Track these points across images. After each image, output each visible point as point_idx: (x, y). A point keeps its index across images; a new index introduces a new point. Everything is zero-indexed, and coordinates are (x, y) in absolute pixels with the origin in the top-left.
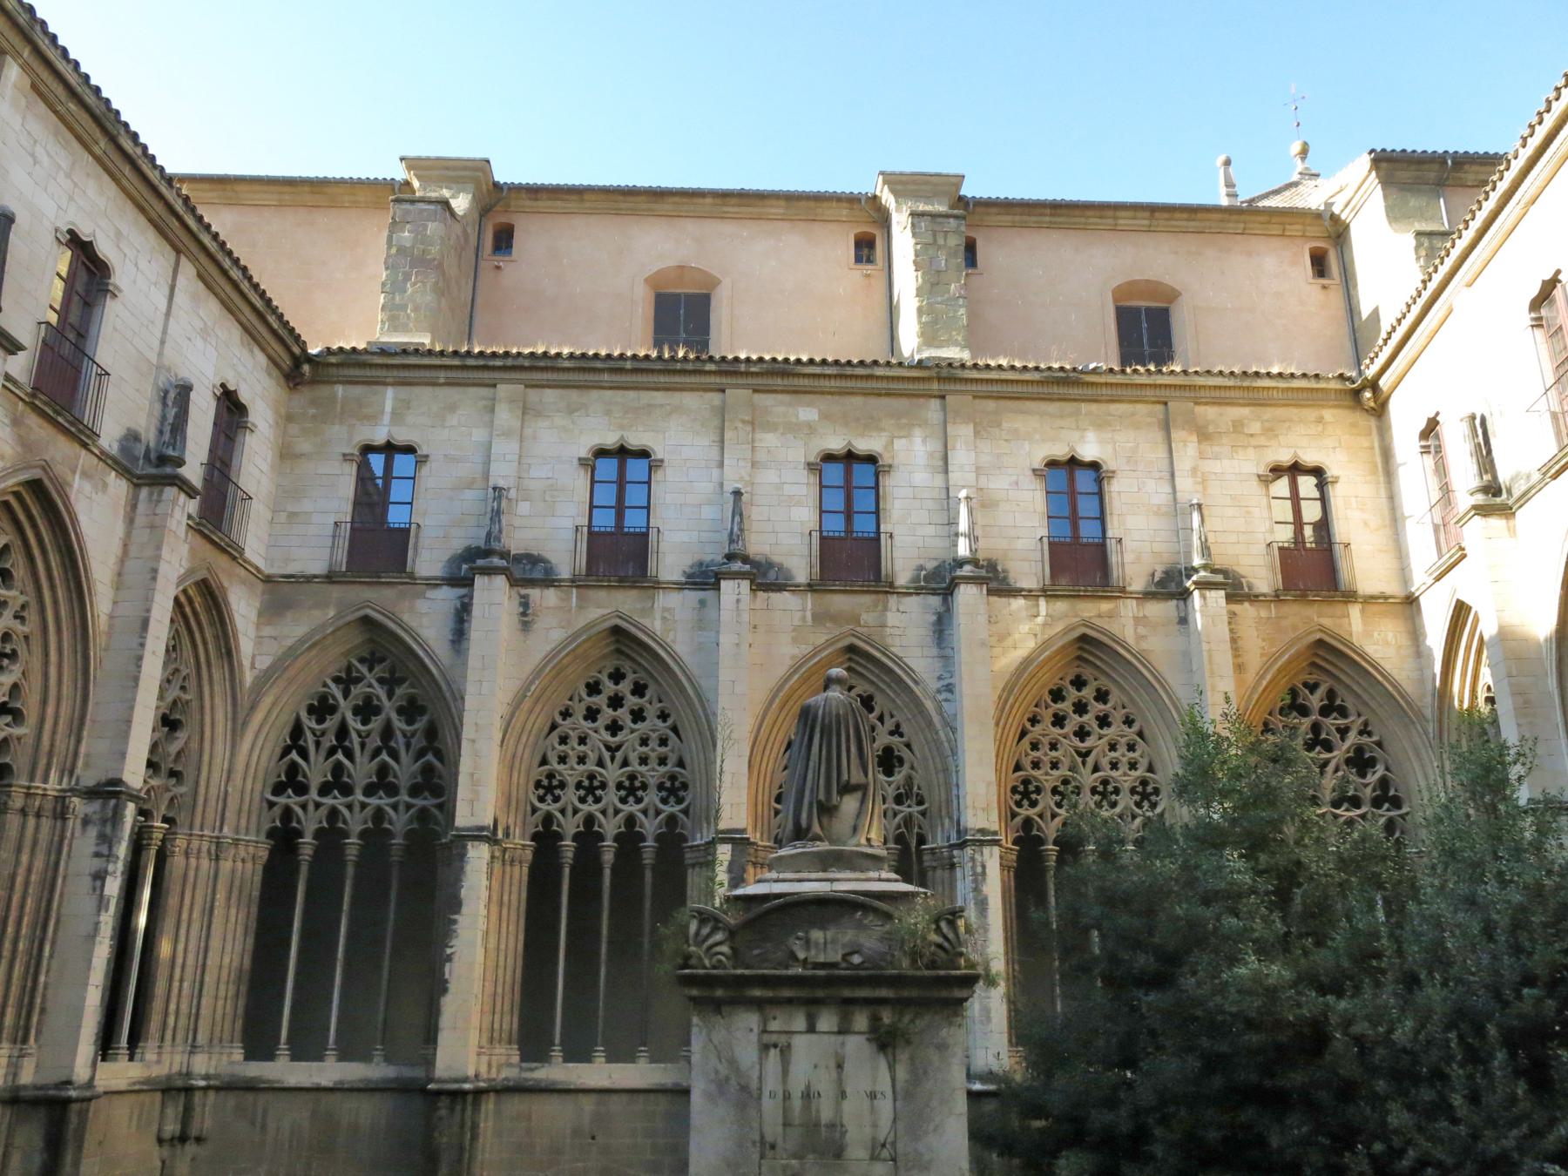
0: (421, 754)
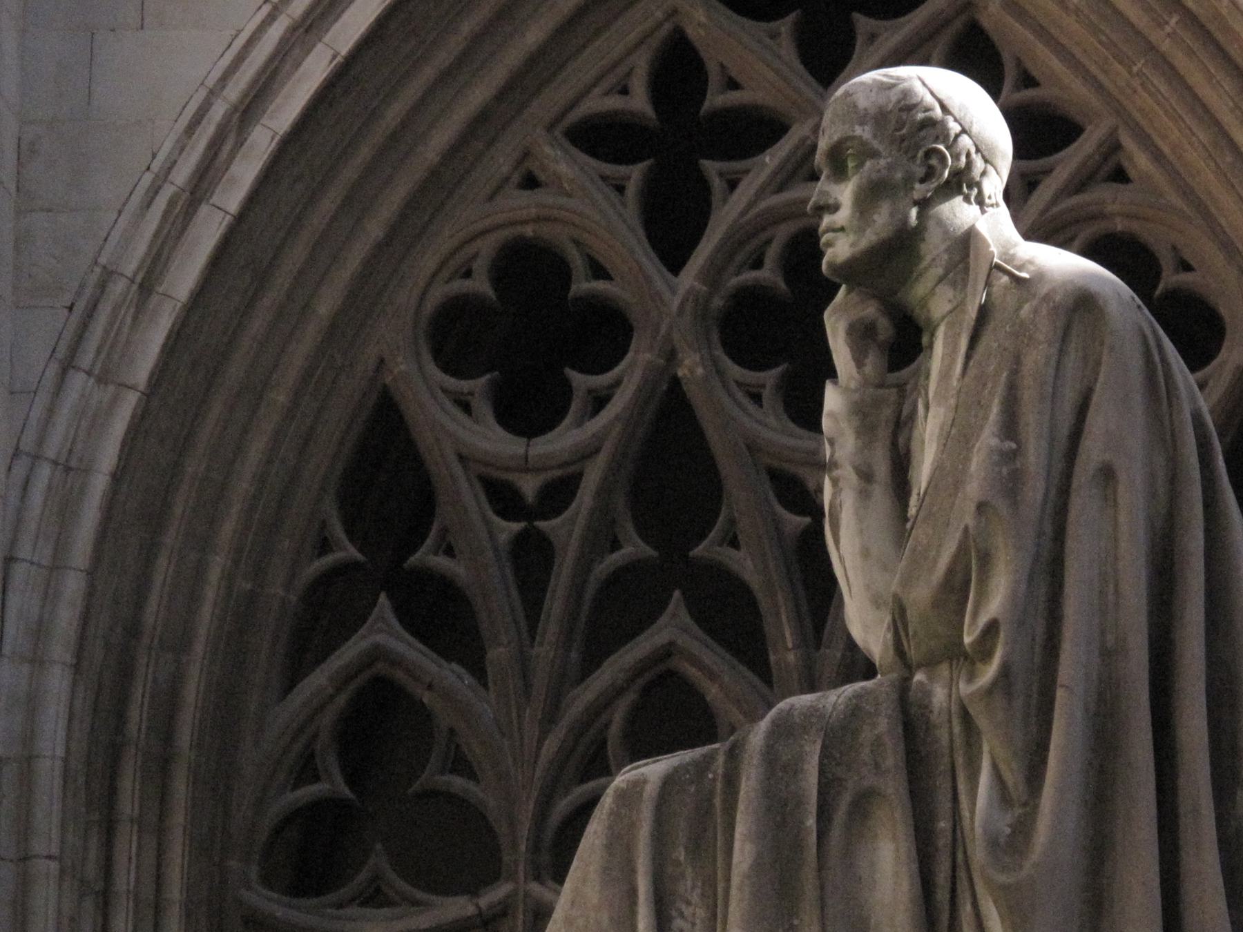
0: (618, 609)
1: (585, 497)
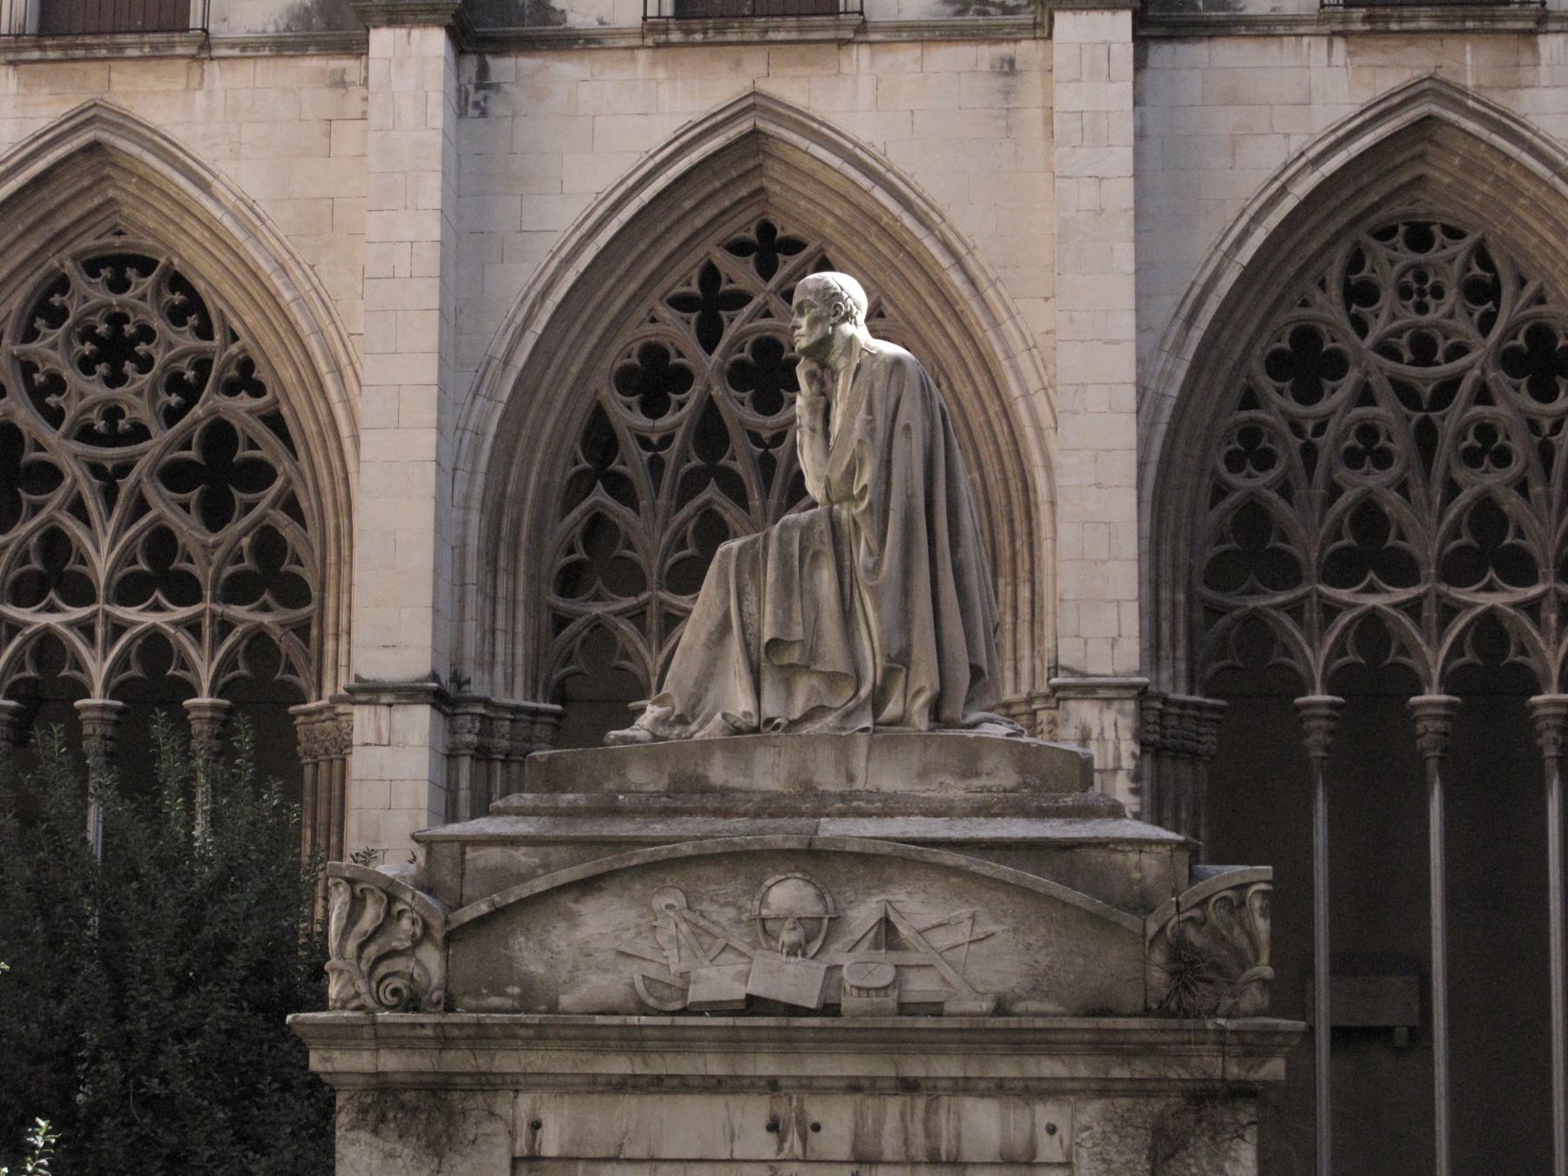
0: (690, 486)
1: (677, 443)
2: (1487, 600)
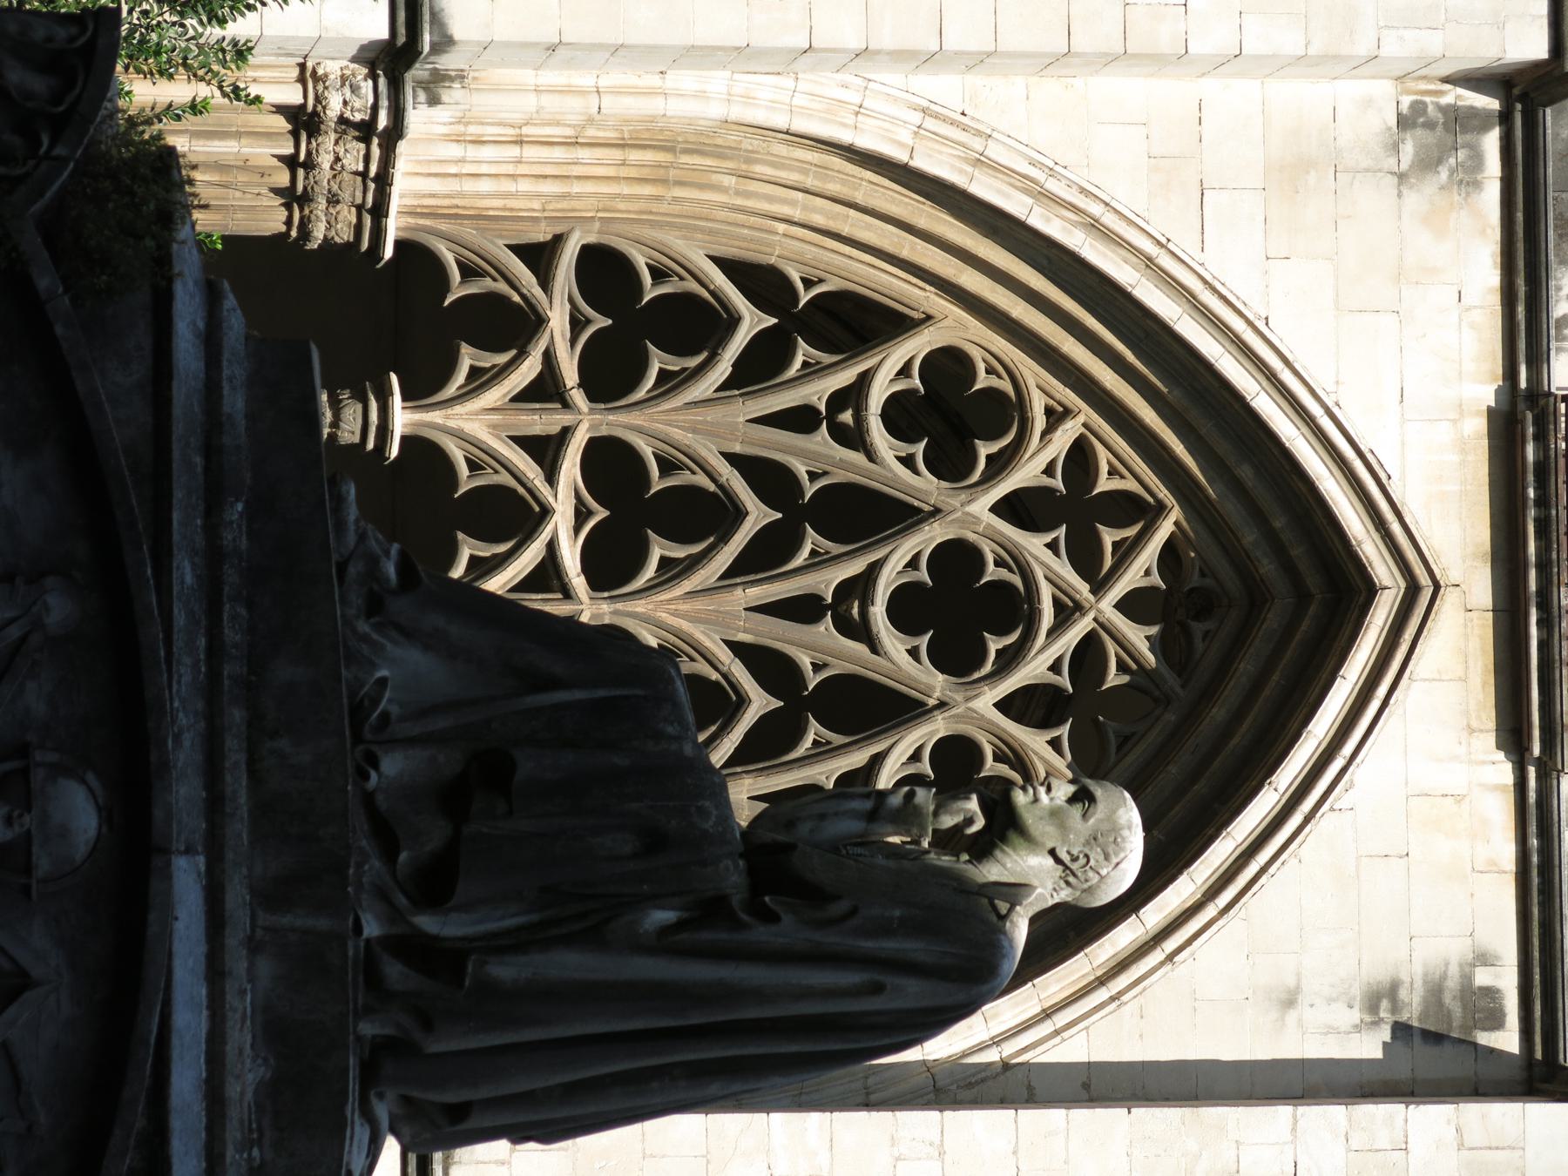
0: (769, 665)
2: (558, 320)
